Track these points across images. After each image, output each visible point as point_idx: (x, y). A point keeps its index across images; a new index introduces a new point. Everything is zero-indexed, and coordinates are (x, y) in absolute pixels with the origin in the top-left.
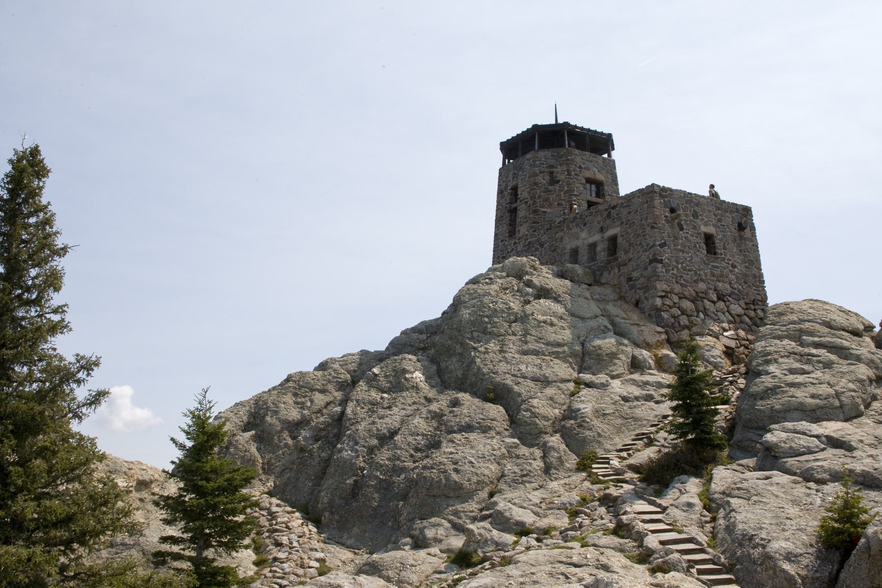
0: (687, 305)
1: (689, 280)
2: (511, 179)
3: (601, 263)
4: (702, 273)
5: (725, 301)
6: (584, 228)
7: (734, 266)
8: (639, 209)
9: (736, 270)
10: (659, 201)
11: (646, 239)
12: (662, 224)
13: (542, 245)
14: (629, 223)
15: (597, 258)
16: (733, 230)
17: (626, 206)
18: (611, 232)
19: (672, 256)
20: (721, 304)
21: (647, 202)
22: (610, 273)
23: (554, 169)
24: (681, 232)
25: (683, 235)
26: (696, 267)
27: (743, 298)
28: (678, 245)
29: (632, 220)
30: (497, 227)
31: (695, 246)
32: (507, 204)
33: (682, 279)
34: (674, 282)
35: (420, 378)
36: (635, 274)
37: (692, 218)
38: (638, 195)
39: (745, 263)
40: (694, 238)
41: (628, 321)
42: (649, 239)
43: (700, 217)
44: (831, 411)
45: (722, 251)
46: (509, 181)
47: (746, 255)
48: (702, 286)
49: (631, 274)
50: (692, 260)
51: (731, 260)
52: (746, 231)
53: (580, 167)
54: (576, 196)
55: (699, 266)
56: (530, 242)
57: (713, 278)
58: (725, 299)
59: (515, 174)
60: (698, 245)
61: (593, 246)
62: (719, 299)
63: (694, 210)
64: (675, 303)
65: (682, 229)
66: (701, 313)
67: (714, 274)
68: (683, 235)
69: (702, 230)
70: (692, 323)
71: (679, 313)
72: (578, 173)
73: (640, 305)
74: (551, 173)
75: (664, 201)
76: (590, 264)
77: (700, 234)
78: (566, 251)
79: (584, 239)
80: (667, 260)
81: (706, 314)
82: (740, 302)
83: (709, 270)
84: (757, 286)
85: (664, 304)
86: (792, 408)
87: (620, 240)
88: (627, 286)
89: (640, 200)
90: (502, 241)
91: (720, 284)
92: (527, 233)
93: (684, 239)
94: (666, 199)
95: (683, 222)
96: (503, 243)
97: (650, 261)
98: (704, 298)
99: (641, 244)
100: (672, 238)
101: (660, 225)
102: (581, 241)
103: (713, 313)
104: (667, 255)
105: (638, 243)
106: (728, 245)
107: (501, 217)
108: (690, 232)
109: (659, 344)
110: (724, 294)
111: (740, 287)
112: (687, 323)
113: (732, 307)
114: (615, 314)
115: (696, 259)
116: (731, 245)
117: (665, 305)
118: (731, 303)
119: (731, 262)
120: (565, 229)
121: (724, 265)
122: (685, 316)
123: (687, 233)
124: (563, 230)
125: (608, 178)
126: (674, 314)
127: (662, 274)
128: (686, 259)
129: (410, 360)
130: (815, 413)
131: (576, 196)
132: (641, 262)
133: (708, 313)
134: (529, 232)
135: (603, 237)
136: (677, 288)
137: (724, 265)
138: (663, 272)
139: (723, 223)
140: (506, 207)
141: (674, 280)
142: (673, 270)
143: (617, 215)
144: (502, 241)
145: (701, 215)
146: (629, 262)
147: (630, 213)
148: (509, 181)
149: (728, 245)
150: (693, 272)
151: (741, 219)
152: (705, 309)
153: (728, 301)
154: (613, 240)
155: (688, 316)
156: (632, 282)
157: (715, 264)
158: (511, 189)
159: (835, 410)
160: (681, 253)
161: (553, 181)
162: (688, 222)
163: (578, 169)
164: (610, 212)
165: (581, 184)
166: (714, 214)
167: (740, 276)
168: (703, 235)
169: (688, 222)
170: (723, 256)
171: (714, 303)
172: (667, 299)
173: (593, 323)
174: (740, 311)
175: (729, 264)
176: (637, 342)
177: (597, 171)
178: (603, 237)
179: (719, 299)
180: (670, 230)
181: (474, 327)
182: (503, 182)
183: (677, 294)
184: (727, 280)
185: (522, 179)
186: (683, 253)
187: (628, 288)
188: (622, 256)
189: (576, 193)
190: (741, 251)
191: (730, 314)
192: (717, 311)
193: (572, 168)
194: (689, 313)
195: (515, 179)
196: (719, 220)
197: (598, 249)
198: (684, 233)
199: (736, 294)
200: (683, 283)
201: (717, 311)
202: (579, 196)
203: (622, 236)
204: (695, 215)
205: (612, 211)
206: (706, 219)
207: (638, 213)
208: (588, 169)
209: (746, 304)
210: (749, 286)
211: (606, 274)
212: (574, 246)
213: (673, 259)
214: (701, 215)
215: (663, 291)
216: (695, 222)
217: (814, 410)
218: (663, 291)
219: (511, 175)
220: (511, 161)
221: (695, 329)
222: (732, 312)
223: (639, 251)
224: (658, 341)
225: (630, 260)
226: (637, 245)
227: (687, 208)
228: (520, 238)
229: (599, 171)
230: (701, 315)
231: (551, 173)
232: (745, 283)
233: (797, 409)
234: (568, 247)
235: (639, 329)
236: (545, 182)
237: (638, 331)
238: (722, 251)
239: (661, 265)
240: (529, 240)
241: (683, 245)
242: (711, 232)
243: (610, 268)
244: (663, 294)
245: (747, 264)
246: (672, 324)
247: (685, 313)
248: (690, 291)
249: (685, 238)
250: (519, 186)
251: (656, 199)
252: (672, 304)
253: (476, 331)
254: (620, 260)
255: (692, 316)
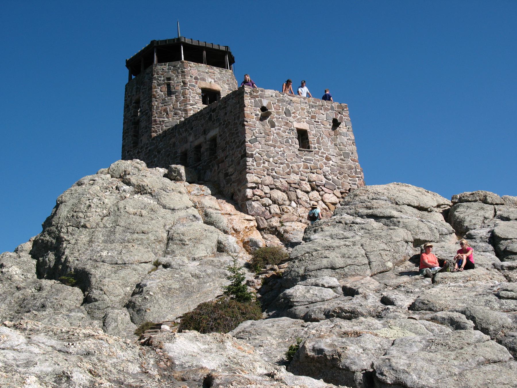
0: (278, 194)
1: (282, 172)
2: (135, 93)
3: (204, 163)
4: (294, 165)
5: (319, 191)
6: (191, 132)
7: (328, 159)
8: (233, 110)
9: (331, 162)
10: (250, 101)
11: (238, 136)
12: (253, 122)
13: (159, 152)
14: (226, 123)
15: (202, 159)
16: (328, 126)
17: (223, 108)
18: (212, 133)
19: (263, 151)
20: (315, 194)
21: (239, 103)
22: (211, 171)
23: (171, 81)
24: (272, 129)
25: (275, 132)
26: (288, 160)
27: (339, 188)
28: (269, 141)
29: (228, 120)
30: (124, 139)
31: (287, 142)
32: (132, 117)
33: (274, 172)
34: (266, 175)
35: (15, 271)
36: (231, 170)
37: (284, 115)
38: (232, 96)
39: (341, 155)
40: (287, 133)
41: (219, 212)
42: (241, 136)
43: (293, 115)
44: (359, 268)
45: (316, 145)
46: (133, 95)
47: (341, 148)
48: (294, 178)
49: (228, 169)
50: (284, 154)
51: (325, 153)
52: (340, 126)
53: (196, 78)
54: (191, 105)
55: (291, 159)
56: (150, 150)
57: (306, 170)
58: (319, 189)
59: (137, 88)
60: (290, 141)
61: (199, 147)
62: (313, 189)
63: (286, 108)
64: (265, 193)
65: (273, 126)
66: (293, 202)
67: (307, 166)
68: (275, 132)
69: (295, 127)
70: (283, 211)
71: (271, 202)
72: (194, 84)
73: (235, 198)
74: (169, 85)
75: (255, 101)
76: (196, 165)
77: (293, 130)
78: (178, 155)
79: (192, 142)
80: (257, 154)
81: (298, 203)
82: (335, 191)
83: (302, 163)
84: (353, 177)
85: (254, 195)
86: (323, 267)
87: (219, 140)
88: (224, 181)
89: (233, 101)
90: (128, 152)
91: (314, 176)
92: (147, 142)
93: (275, 135)
94: (257, 99)
95: (274, 120)
96: (129, 153)
97: (241, 156)
98: (297, 188)
99: (234, 141)
100: (263, 134)
101: (251, 123)
102: (189, 144)
103: (306, 202)
104: (258, 150)
105: (233, 140)
106: (322, 139)
107: (128, 129)
108: (282, 129)
109: (247, 230)
110: (317, 184)
111: (335, 178)
112: (278, 211)
113: (326, 196)
114: (208, 206)
115: (287, 153)
116: (326, 139)
117: (257, 195)
118: (325, 193)
119: (325, 155)
120: (177, 135)
121: (318, 158)
122: (276, 205)
123: (280, 129)
124: (175, 135)
125: (225, 88)
126: (265, 204)
127: (253, 167)
128: (278, 153)
129: (10, 256)
130: (344, 270)
131: (191, 105)
132: (235, 158)
133: (300, 202)
134: (149, 141)
135: (205, 139)
136: (268, 180)
137: (317, 157)
138: (254, 166)
139: (317, 120)
140: (131, 120)
141: (266, 172)
142: (264, 163)
143: (216, 117)
144: (128, 152)
145: (294, 113)
146: (225, 159)
147: (226, 114)
148: (133, 95)
149: (322, 139)
150: (285, 165)
151: (336, 116)
152: (297, 198)
153: (323, 190)
154: (214, 140)
155: (279, 205)
156: (228, 177)
157: (308, 157)
158: (135, 103)
159: (363, 267)
160: (272, 148)
161: (170, 93)
162: (280, 119)
163: (194, 80)
164: (211, 114)
165: (197, 94)
166: (308, 112)
167: (335, 168)
168: (295, 131)
169: (280, 119)
170: (317, 150)
171: (307, 192)
172: (257, 190)
173: (182, 214)
174: (334, 199)
175: (322, 156)
176: (226, 229)
177: (213, 81)
178: (205, 139)
179: (313, 189)
180: (261, 126)
181: (70, 223)
182: (129, 97)
183: (268, 185)
184: (321, 171)
185: (143, 93)
186: (275, 147)
187: (225, 183)
188: (221, 155)
189: (191, 102)
190: (335, 145)
191: (325, 203)
192: (310, 200)
193: (188, 79)
194: (281, 202)
195: (138, 93)
196: (312, 117)
197: (202, 150)
198: (275, 130)
199: (331, 184)
200: (274, 176)
201: (310, 200)
202: (194, 105)
203: (220, 136)
204: (288, 113)
205: (212, 114)
206: (299, 117)
207: (232, 113)
208: (203, 79)
209: (342, 193)
210: (344, 177)
211: (208, 173)
212: (184, 150)
213: (264, 154)
214: (294, 113)
215: (254, 182)
216: (287, 120)
217: (343, 268)
218: (254, 182)
219: (134, 90)
220: (133, 77)
221: (285, 216)
222: (327, 201)
223: (233, 149)
224: (246, 227)
225: (226, 157)
226: (231, 142)
227: (279, 106)
228: (142, 148)
229: (215, 81)
230: (294, 204)
231: (169, 85)
232: (340, 174)
233: (327, 268)
234: (179, 151)
235: (229, 218)
236: (162, 93)
237: (228, 220)
238: (316, 145)
239: (251, 159)
240: (149, 148)
241: (275, 141)
242: (304, 128)
243: (211, 167)
244: (254, 185)
245: (342, 157)
246: (263, 212)
247: (277, 202)
248: (282, 183)
249: (277, 134)
250: (141, 99)
251: (246, 99)
252: (263, 194)
253: (71, 225)
254: (219, 158)
255: (283, 204)
